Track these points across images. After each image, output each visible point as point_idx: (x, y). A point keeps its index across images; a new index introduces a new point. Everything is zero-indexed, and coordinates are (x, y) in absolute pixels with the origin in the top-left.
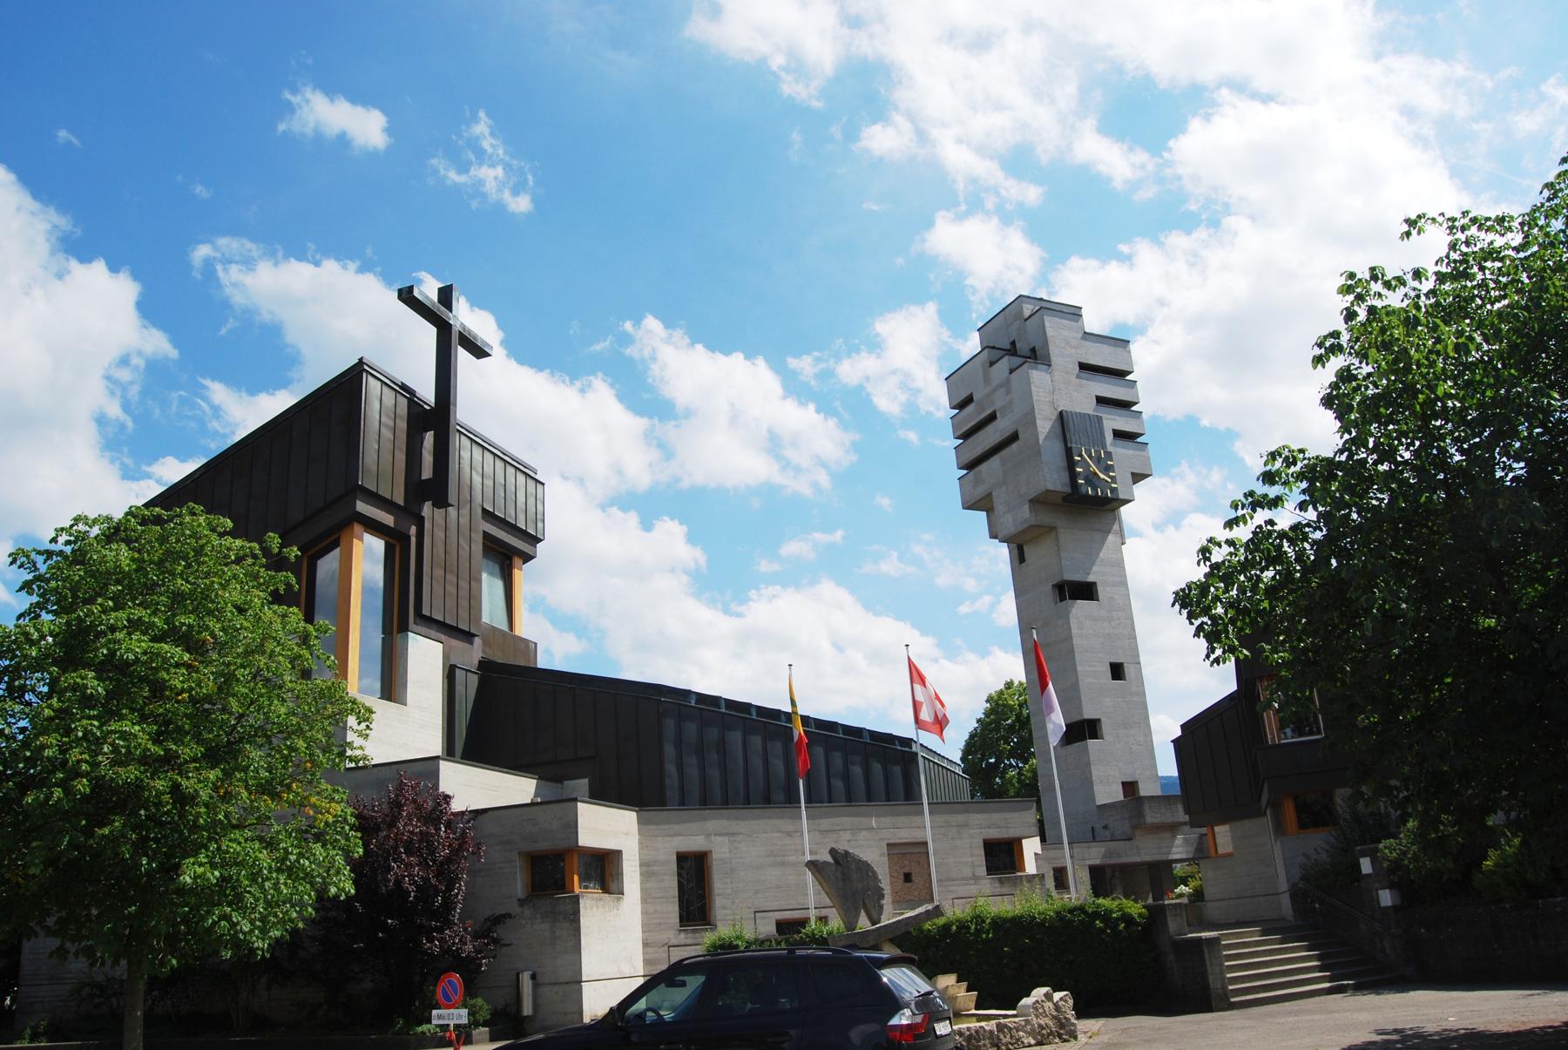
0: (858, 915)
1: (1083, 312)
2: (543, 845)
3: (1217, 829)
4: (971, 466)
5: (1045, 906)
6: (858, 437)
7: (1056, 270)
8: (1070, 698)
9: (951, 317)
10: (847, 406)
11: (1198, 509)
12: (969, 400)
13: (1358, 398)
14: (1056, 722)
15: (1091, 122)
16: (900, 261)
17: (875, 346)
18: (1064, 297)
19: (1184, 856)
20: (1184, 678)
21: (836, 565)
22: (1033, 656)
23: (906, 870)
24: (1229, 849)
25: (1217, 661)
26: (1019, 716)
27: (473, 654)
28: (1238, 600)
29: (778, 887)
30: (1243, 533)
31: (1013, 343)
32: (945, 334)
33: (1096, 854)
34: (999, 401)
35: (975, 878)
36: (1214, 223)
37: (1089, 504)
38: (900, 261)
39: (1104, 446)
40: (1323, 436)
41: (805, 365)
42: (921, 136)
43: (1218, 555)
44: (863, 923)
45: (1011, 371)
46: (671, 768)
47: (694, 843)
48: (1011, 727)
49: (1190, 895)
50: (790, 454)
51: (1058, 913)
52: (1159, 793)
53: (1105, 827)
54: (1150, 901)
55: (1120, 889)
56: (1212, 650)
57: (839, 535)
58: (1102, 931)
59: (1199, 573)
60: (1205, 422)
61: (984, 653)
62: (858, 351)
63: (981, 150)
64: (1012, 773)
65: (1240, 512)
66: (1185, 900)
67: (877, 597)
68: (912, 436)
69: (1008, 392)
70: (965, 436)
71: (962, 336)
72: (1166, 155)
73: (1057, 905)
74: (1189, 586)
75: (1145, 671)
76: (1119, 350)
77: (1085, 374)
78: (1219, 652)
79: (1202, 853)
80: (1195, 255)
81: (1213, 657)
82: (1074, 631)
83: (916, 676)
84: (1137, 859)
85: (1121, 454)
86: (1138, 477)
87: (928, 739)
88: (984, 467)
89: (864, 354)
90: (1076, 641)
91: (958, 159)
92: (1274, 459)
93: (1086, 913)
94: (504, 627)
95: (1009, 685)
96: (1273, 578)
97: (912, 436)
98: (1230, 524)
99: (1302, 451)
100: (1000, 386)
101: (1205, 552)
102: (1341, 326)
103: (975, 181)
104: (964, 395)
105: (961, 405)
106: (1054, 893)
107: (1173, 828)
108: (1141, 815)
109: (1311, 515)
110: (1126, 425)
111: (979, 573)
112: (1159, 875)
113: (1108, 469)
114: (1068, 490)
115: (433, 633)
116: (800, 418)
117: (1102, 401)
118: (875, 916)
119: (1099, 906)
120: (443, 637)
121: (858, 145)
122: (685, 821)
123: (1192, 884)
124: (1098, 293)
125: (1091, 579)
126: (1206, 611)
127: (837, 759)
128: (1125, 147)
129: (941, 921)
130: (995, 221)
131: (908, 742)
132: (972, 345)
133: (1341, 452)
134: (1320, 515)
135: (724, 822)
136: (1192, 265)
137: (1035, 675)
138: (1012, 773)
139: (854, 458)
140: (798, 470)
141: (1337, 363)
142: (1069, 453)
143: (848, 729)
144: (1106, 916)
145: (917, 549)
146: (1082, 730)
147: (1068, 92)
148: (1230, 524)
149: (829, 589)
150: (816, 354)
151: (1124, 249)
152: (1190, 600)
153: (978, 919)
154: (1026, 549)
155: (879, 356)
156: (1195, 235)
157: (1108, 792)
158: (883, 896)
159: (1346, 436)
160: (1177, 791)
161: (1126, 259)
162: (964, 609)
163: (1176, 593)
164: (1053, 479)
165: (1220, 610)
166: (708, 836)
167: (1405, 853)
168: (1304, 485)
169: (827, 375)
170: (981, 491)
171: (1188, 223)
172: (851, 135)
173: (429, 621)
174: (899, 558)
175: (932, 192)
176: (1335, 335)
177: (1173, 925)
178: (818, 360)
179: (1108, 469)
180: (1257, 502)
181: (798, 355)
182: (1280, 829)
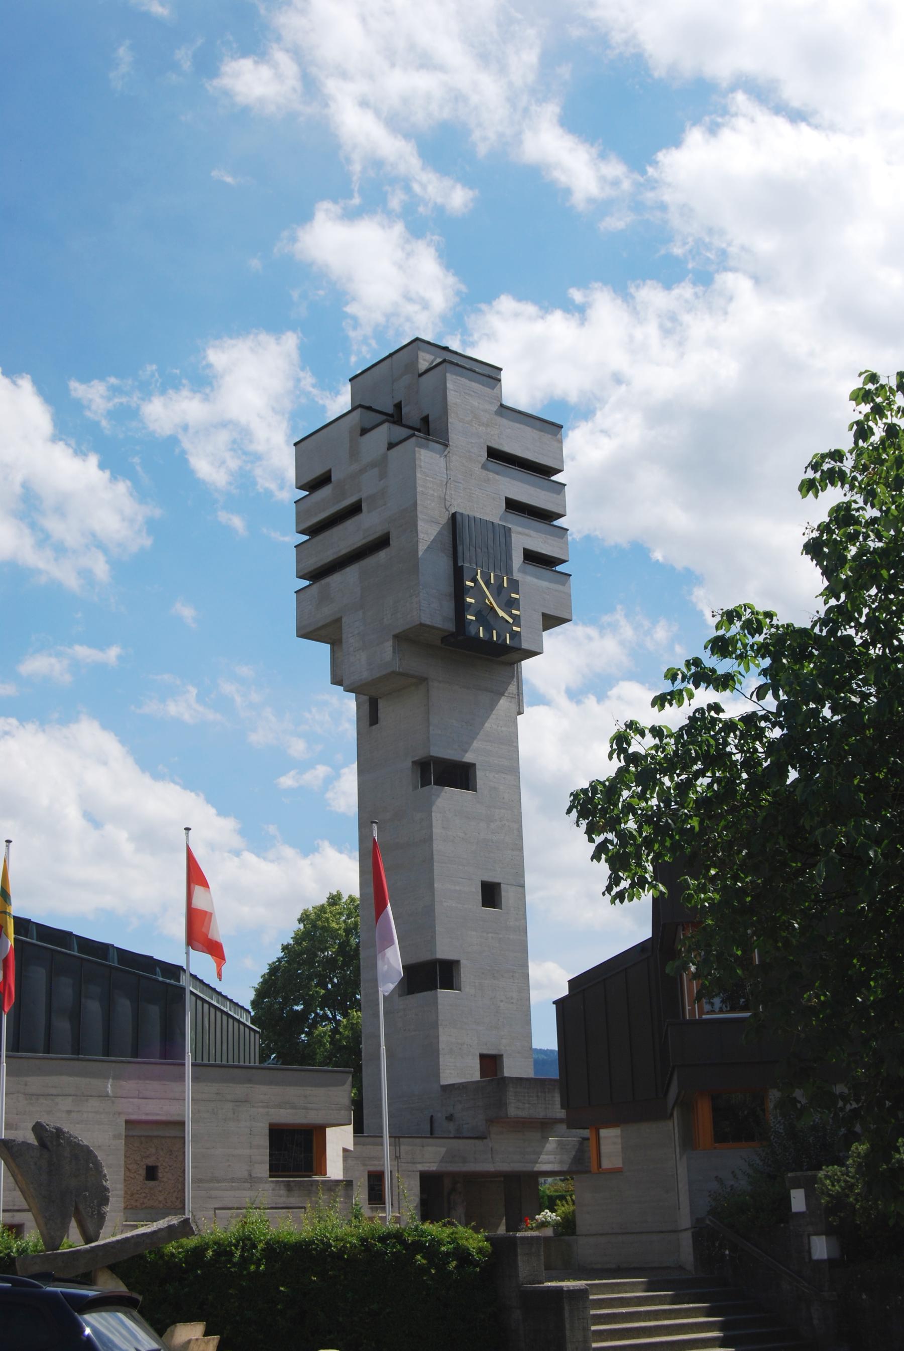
0: (65, 1229)
1: (504, 375)
3: (603, 1132)
4: (316, 575)
5: (346, 1228)
6: (158, 513)
7: (480, 311)
8: (418, 926)
9: (315, 357)
10: (149, 464)
11: (631, 677)
12: (323, 480)
13: (853, 550)
14: (392, 962)
15: (551, 110)
16: (255, 264)
17: (204, 382)
18: (483, 353)
19: (555, 1167)
20: (578, 916)
21: (106, 699)
22: (370, 862)
23: (150, 1162)
24: (618, 1163)
25: (620, 896)
26: (344, 945)
28: (659, 813)
30: (675, 717)
31: (398, 406)
32: (308, 380)
33: (431, 1156)
34: (367, 487)
35: (252, 1180)
36: (704, 279)
37: (479, 652)
38: (255, 264)
39: (509, 571)
40: (800, 594)
41: (94, 395)
42: (310, 86)
43: (640, 745)
44: (73, 1240)
45: (391, 446)
48: (331, 962)
49: (557, 1225)
50: (54, 526)
51: (363, 1240)
52: (529, 1073)
53: (450, 1118)
54: (502, 1230)
55: (460, 1211)
56: (615, 880)
57: (113, 653)
58: (423, 1270)
59: (607, 768)
60: (658, 555)
61: (308, 849)
62: (177, 387)
63: (395, 122)
64: (325, 1028)
65: (679, 685)
66: (549, 1232)
67: (157, 752)
68: (237, 522)
69: (383, 475)
70: (314, 531)
71: (327, 384)
72: (650, 170)
73: (365, 1228)
74: (593, 787)
75: (531, 899)
76: (547, 437)
77: (494, 465)
78: (625, 884)
79: (581, 1164)
80: (673, 317)
81: (616, 890)
82: (437, 830)
83: (195, 875)
84: (489, 1167)
85: (532, 584)
86: (551, 621)
87: (201, 965)
88: (335, 580)
89: (185, 393)
90: (438, 846)
91: (358, 127)
92: (731, 622)
93: (403, 1242)
95: (334, 900)
96: (710, 786)
97: (237, 522)
98: (660, 701)
99: (769, 615)
100: (373, 465)
101: (620, 741)
102: (846, 442)
103: (377, 163)
104: (318, 471)
105: (314, 484)
106: (366, 1211)
107: (544, 1126)
108: (501, 1104)
109: (770, 703)
110: (543, 545)
111: (316, 730)
112: (519, 1192)
113: (510, 604)
114: (451, 627)
116: (74, 473)
117: (513, 505)
118: (91, 1229)
119: (423, 1233)
121: (216, 82)
123: (563, 1208)
124: (531, 352)
125: (469, 758)
126: (613, 824)
127: (66, 988)
128: (594, 151)
129: (191, 1242)
130: (399, 228)
131: (174, 971)
132: (341, 402)
133: (823, 622)
134: (781, 706)
136: (666, 332)
137: (371, 890)
138: (325, 1028)
139: (148, 542)
140: (60, 550)
141: (834, 495)
142: (458, 574)
143: (87, 945)
144: (431, 1249)
145: (228, 688)
146: (430, 975)
147: (525, 60)
148: (660, 701)
149: (89, 733)
150: (113, 380)
151: (577, 295)
152: (593, 807)
153: (247, 1242)
154: (381, 704)
155: (206, 399)
156: (676, 292)
157: (459, 1068)
158: (105, 1201)
159: (833, 602)
160: (554, 1073)
161: (580, 312)
162: (287, 781)
163: (575, 795)
164: (430, 608)
165: (631, 825)
167: (851, 1187)
168: (767, 662)
169: (126, 415)
170: (326, 613)
171: (669, 273)
172: (207, 65)
174: (200, 699)
175: (307, 168)
176: (837, 455)
177: (526, 1267)
178: (115, 391)
179: (510, 604)
180: (702, 676)
181: (85, 379)
182: (688, 1141)
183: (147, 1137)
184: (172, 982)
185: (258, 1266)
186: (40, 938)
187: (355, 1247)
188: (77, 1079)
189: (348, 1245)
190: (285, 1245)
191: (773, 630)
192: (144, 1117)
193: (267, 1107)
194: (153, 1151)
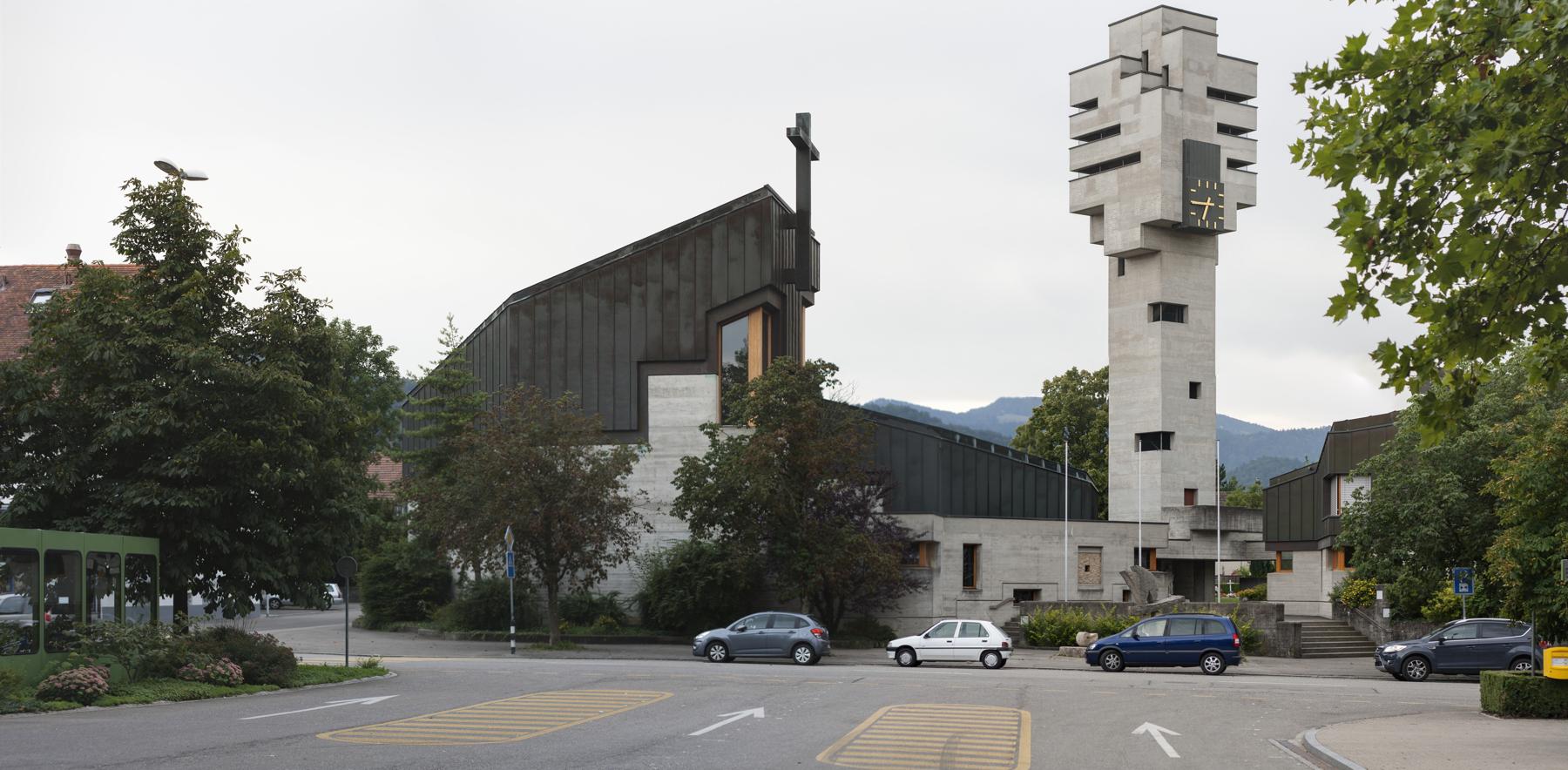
12: (1091, 105)
34: (1124, 117)
47: (972, 539)
69: (1137, 111)
88: (1100, 178)
100: (1129, 101)
170: (1091, 202)
191: (1317, 147)
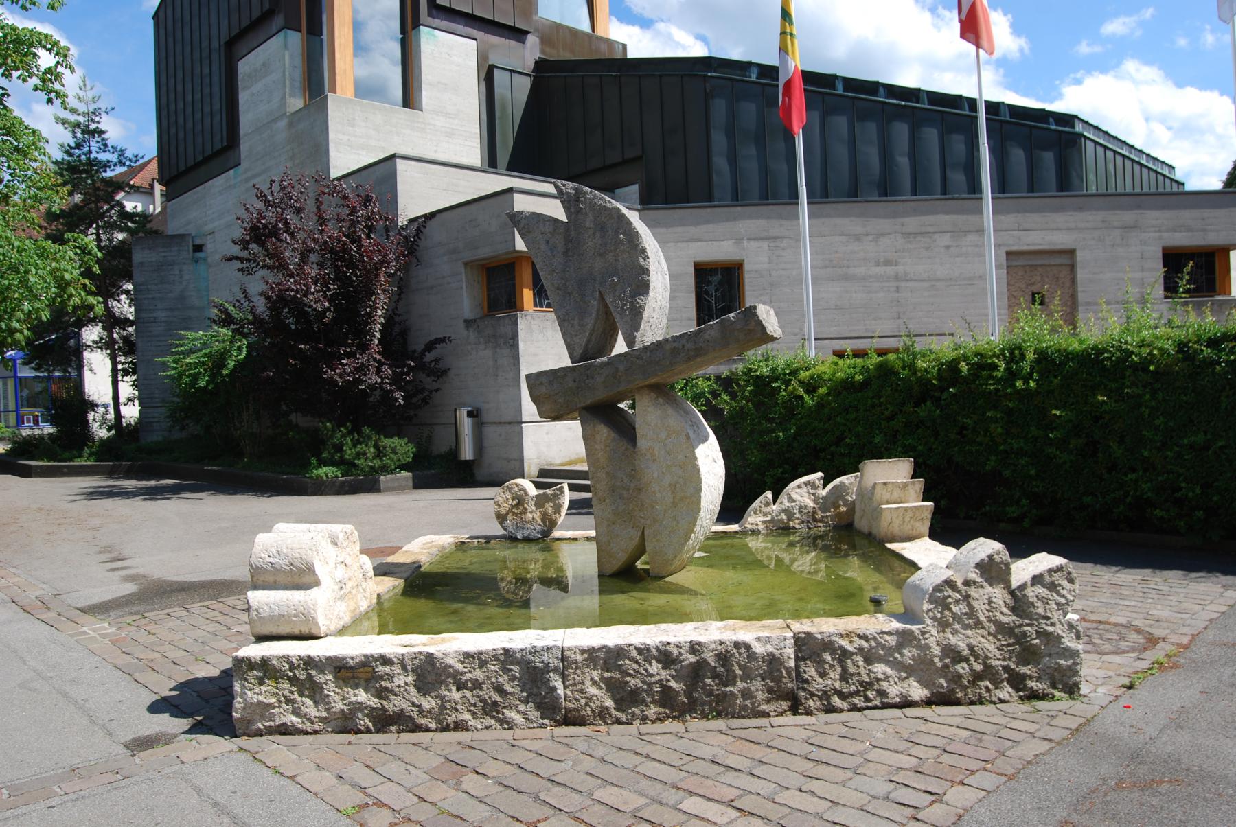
2: (484, 252)
27: (530, 52)
29: (837, 308)
46: (720, 163)
47: (718, 250)
51: (1181, 346)
94: (585, 26)
115: (460, 28)
120: (479, 34)
122: (708, 222)
135: (762, 223)
166: (739, 241)
173: (451, 14)
183: (1031, 266)
184: (1066, 129)
185: (1026, 382)
186: (930, 103)
187: (1169, 354)
188: (955, 216)
189: (1155, 352)
190: (1068, 354)
192: (1025, 248)
193: (1160, 231)
194: (1038, 278)
